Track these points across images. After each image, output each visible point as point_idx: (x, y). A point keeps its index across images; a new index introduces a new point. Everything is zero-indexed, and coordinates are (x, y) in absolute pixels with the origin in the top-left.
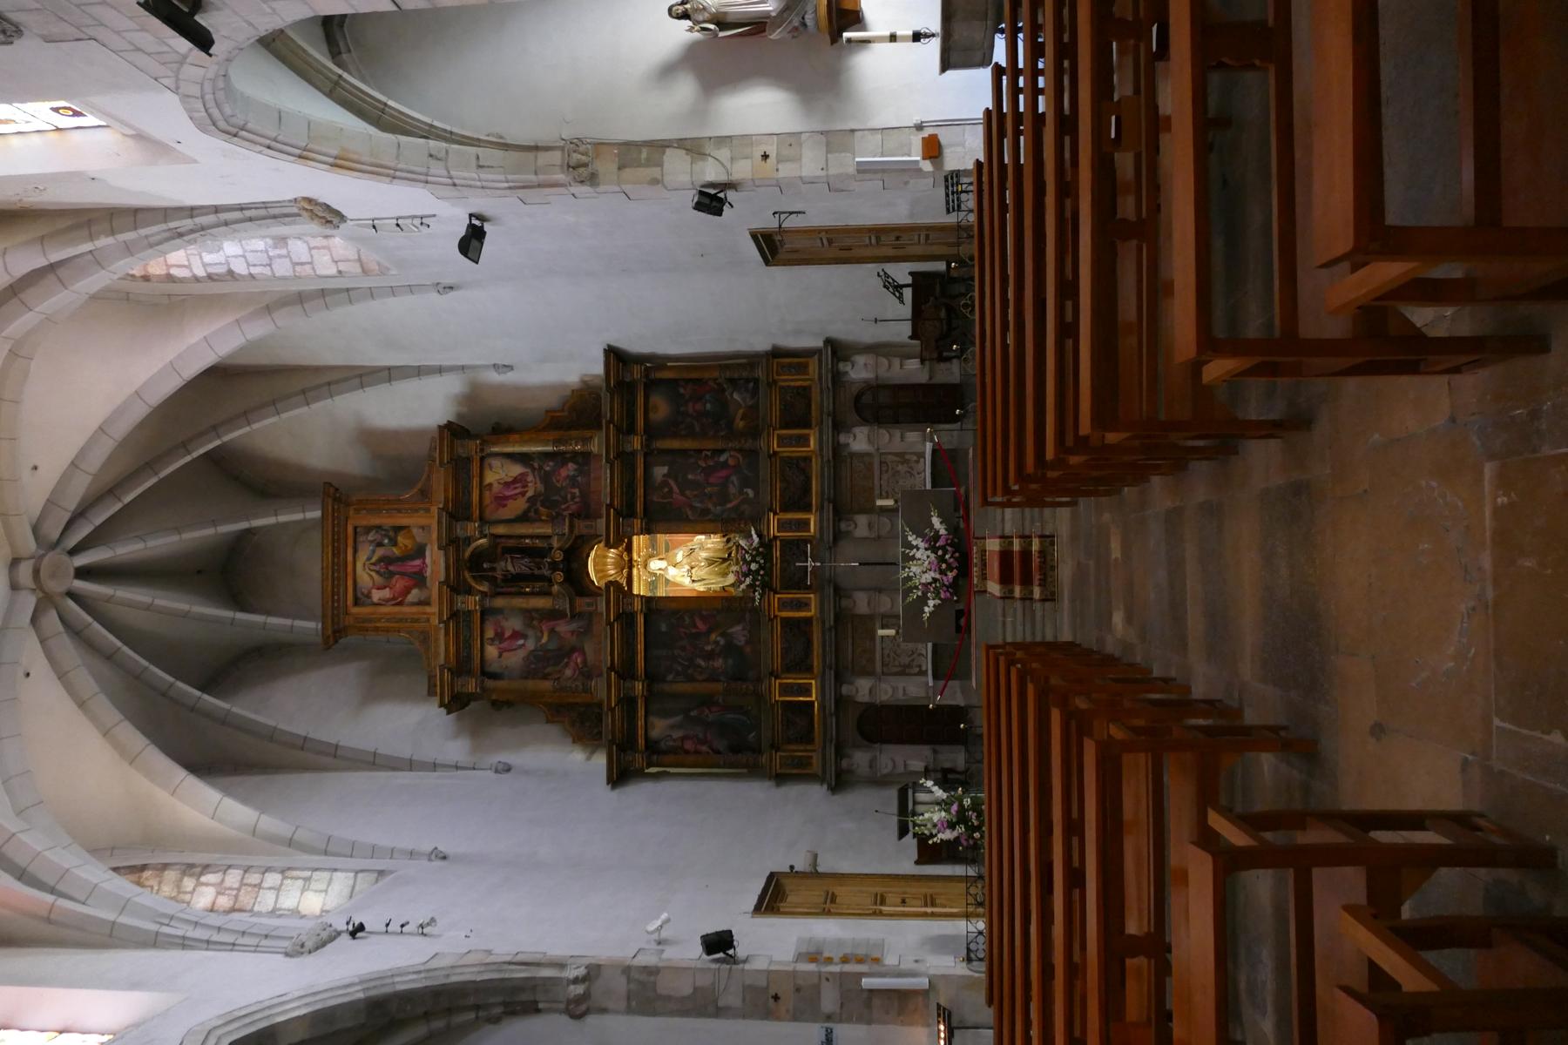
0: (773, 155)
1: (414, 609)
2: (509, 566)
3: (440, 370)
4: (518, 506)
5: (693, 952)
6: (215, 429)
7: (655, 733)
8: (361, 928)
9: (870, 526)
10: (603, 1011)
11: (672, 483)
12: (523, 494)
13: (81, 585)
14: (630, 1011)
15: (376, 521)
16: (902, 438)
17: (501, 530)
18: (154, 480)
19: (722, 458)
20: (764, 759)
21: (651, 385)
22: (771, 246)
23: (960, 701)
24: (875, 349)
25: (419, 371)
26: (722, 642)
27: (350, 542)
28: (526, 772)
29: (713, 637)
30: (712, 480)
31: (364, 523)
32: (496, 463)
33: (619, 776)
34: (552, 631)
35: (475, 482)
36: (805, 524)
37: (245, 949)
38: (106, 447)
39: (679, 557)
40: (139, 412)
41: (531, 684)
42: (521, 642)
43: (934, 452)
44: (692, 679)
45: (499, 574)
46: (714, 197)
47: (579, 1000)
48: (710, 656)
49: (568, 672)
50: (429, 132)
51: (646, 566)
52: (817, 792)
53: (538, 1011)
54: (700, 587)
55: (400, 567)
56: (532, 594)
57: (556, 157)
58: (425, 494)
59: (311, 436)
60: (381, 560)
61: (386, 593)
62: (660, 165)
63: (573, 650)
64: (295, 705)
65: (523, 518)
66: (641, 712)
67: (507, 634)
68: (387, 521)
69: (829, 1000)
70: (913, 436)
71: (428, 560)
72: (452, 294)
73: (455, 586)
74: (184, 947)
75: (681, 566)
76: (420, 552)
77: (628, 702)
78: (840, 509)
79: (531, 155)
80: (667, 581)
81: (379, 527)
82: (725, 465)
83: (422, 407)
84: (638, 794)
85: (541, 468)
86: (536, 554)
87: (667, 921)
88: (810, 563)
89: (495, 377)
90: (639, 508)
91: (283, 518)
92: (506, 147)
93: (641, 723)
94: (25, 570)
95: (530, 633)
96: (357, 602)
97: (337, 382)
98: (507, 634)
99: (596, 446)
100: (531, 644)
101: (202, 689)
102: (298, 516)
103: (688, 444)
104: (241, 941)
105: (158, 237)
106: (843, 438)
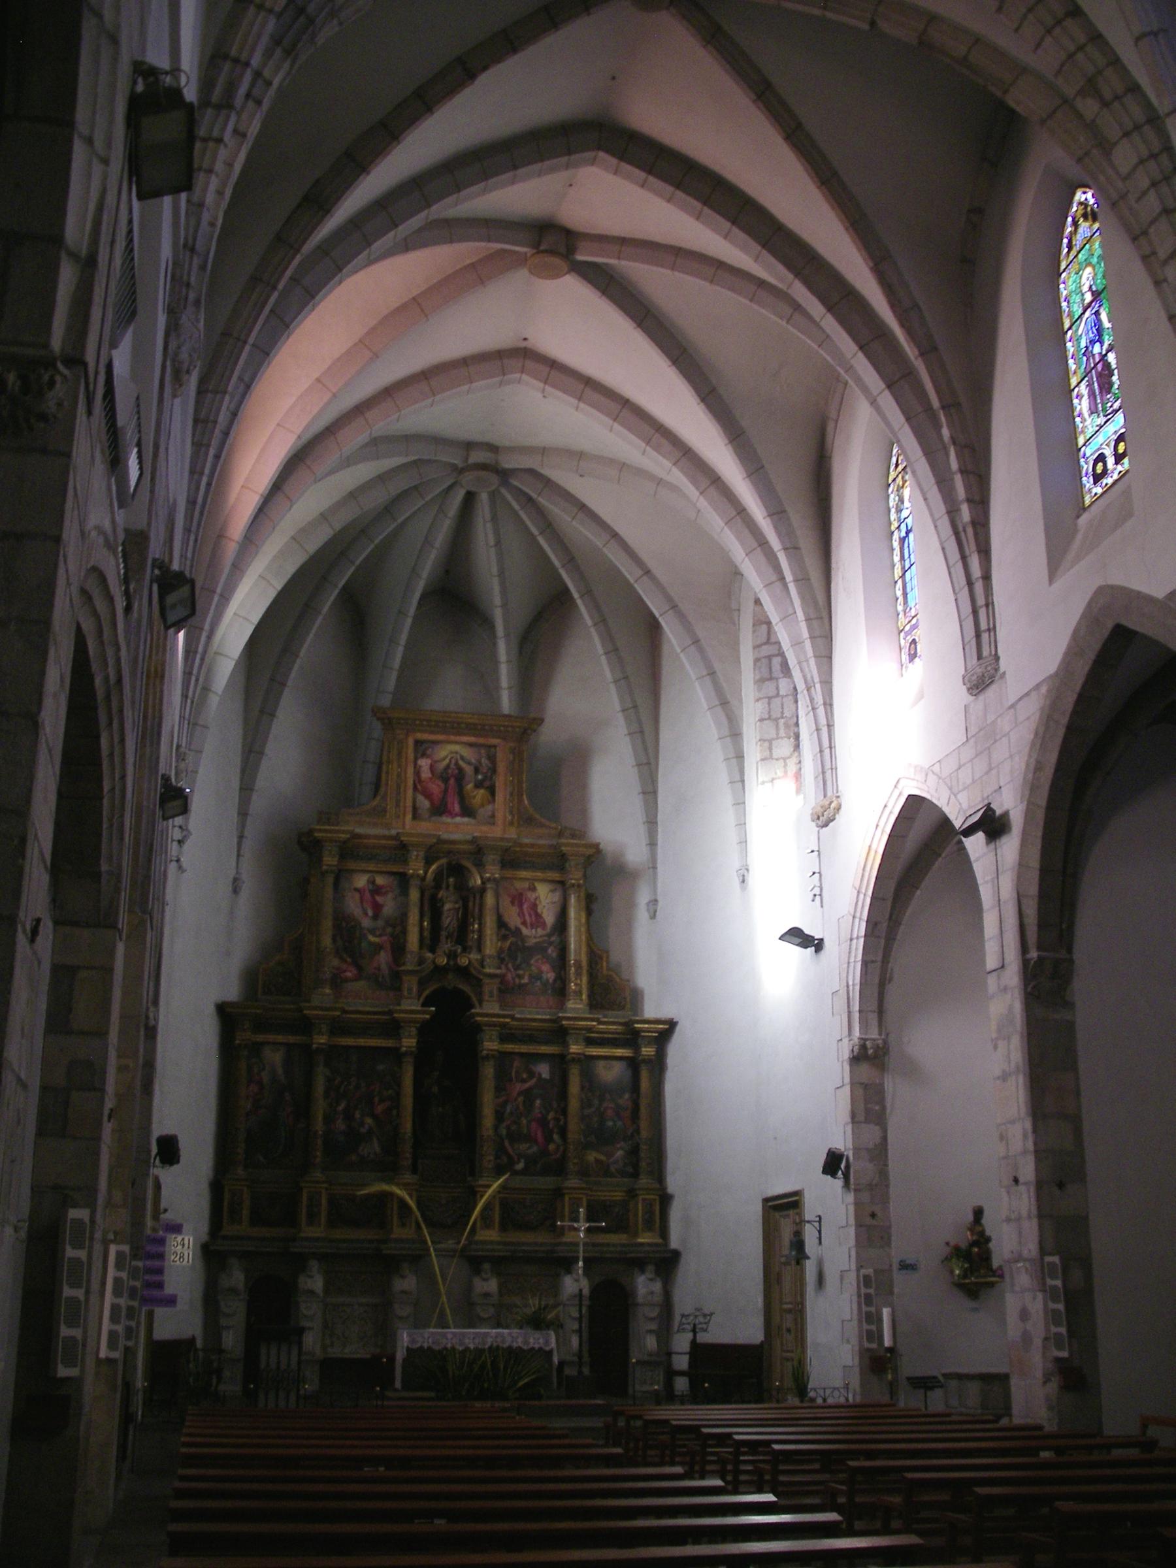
1: (409, 803)
3: (652, 844)
4: (513, 918)
6: (588, 593)
9: (487, 1295)
12: (524, 923)
13: (460, 495)
15: (501, 767)
16: (651, 1331)
17: (490, 899)
18: (557, 563)
19: (556, 1137)
21: (634, 1064)
25: (652, 823)
26: (363, 1130)
27: (481, 741)
30: (534, 1125)
31: (500, 755)
32: (557, 897)
33: (223, 1010)
34: (379, 947)
41: (328, 924)
42: (370, 913)
48: (348, 1116)
49: (336, 962)
55: (453, 790)
56: (421, 928)
58: (529, 821)
59: (583, 693)
60: (460, 769)
61: (426, 774)
63: (360, 968)
65: (501, 924)
66: (291, 1039)
67: (379, 899)
68: (500, 781)
71: (458, 819)
81: (494, 770)
82: (549, 1139)
85: (551, 943)
86: (461, 935)
89: (643, 898)
90: (510, 1047)
91: (504, 670)
93: (280, 1038)
95: (380, 923)
96: (418, 743)
97: (644, 742)
98: (379, 899)
100: (366, 923)
101: (344, 588)
103: (574, 1104)
104: (189, 701)
105: (807, 670)
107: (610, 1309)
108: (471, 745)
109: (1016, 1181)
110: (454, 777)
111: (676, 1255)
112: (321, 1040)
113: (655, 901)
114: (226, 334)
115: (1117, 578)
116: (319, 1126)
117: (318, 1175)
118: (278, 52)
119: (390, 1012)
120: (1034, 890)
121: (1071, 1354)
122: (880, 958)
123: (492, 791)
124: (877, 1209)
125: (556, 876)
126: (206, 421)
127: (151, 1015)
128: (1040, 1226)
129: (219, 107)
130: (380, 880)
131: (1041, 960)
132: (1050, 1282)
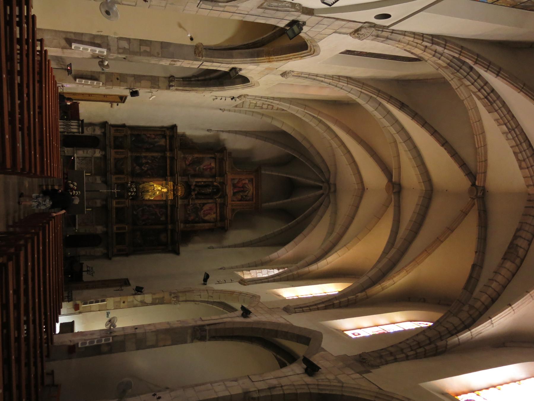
0: (122, 303)
2: (209, 190)
3: (229, 247)
4: (206, 207)
5: (141, 92)
7: (164, 140)
8: (232, 99)
10: (165, 77)
11: (159, 215)
13: (321, 184)
14: (158, 77)
15: (247, 202)
17: (210, 201)
20: (129, 132)
22: (126, 282)
23: (66, 149)
24: (93, 257)
25: (235, 246)
28: (203, 129)
29: (146, 169)
31: (250, 202)
33: (174, 127)
35: (218, 215)
36: (116, 203)
37: (258, 97)
38: (313, 223)
39: (158, 193)
40: (305, 232)
43: (75, 226)
44: (153, 156)
45: (211, 188)
46: (138, 291)
47: (172, 81)
48: (147, 163)
49: (190, 159)
50: (213, 303)
51: (168, 190)
52: (112, 122)
53: (183, 78)
54: (152, 183)
56: (201, 182)
57: (181, 299)
60: (245, 192)
61: (244, 182)
62: (153, 299)
64: (268, 150)
65: (204, 204)
66: (168, 147)
69: (103, 77)
70: (82, 231)
72: (220, 267)
73: (223, 184)
74: (273, 98)
75: (158, 189)
76: (234, 194)
77: (171, 150)
78: (105, 208)
79: (188, 299)
80: (162, 185)
81: (246, 201)
83: (236, 236)
84: (167, 123)
87: (150, 98)
88: (116, 191)
89: (213, 245)
91: (281, 202)
92: (194, 301)
93: (168, 143)
94: (332, 189)
96: (252, 179)
99: (182, 226)
100: (202, 166)
102: (271, 204)
106: (105, 229)
107: (91, 240)
108: (253, 194)
109: (136, 329)
110: (243, 189)
111: (110, 259)
112: (168, 154)
113: (213, 248)
114: (363, 84)
115: (324, 336)
116: (144, 154)
117: (129, 154)
118: (449, 61)
119: (177, 173)
120: (227, 326)
121: (80, 348)
122: (202, 299)
123: (240, 200)
124: (126, 303)
125: (218, 218)
126: (339, 79)
127: (173, 88)
128: (121, 335)
129: (432, 40)
130: (214, 170)
131: (205, 330)
132: (103, 339)
